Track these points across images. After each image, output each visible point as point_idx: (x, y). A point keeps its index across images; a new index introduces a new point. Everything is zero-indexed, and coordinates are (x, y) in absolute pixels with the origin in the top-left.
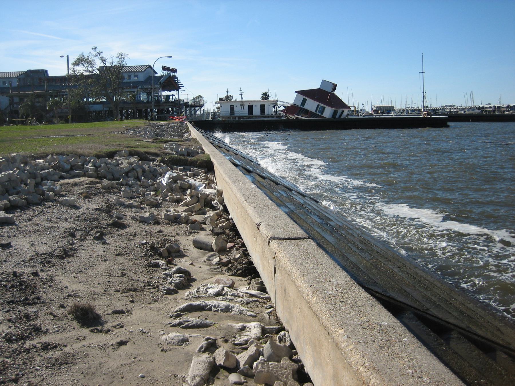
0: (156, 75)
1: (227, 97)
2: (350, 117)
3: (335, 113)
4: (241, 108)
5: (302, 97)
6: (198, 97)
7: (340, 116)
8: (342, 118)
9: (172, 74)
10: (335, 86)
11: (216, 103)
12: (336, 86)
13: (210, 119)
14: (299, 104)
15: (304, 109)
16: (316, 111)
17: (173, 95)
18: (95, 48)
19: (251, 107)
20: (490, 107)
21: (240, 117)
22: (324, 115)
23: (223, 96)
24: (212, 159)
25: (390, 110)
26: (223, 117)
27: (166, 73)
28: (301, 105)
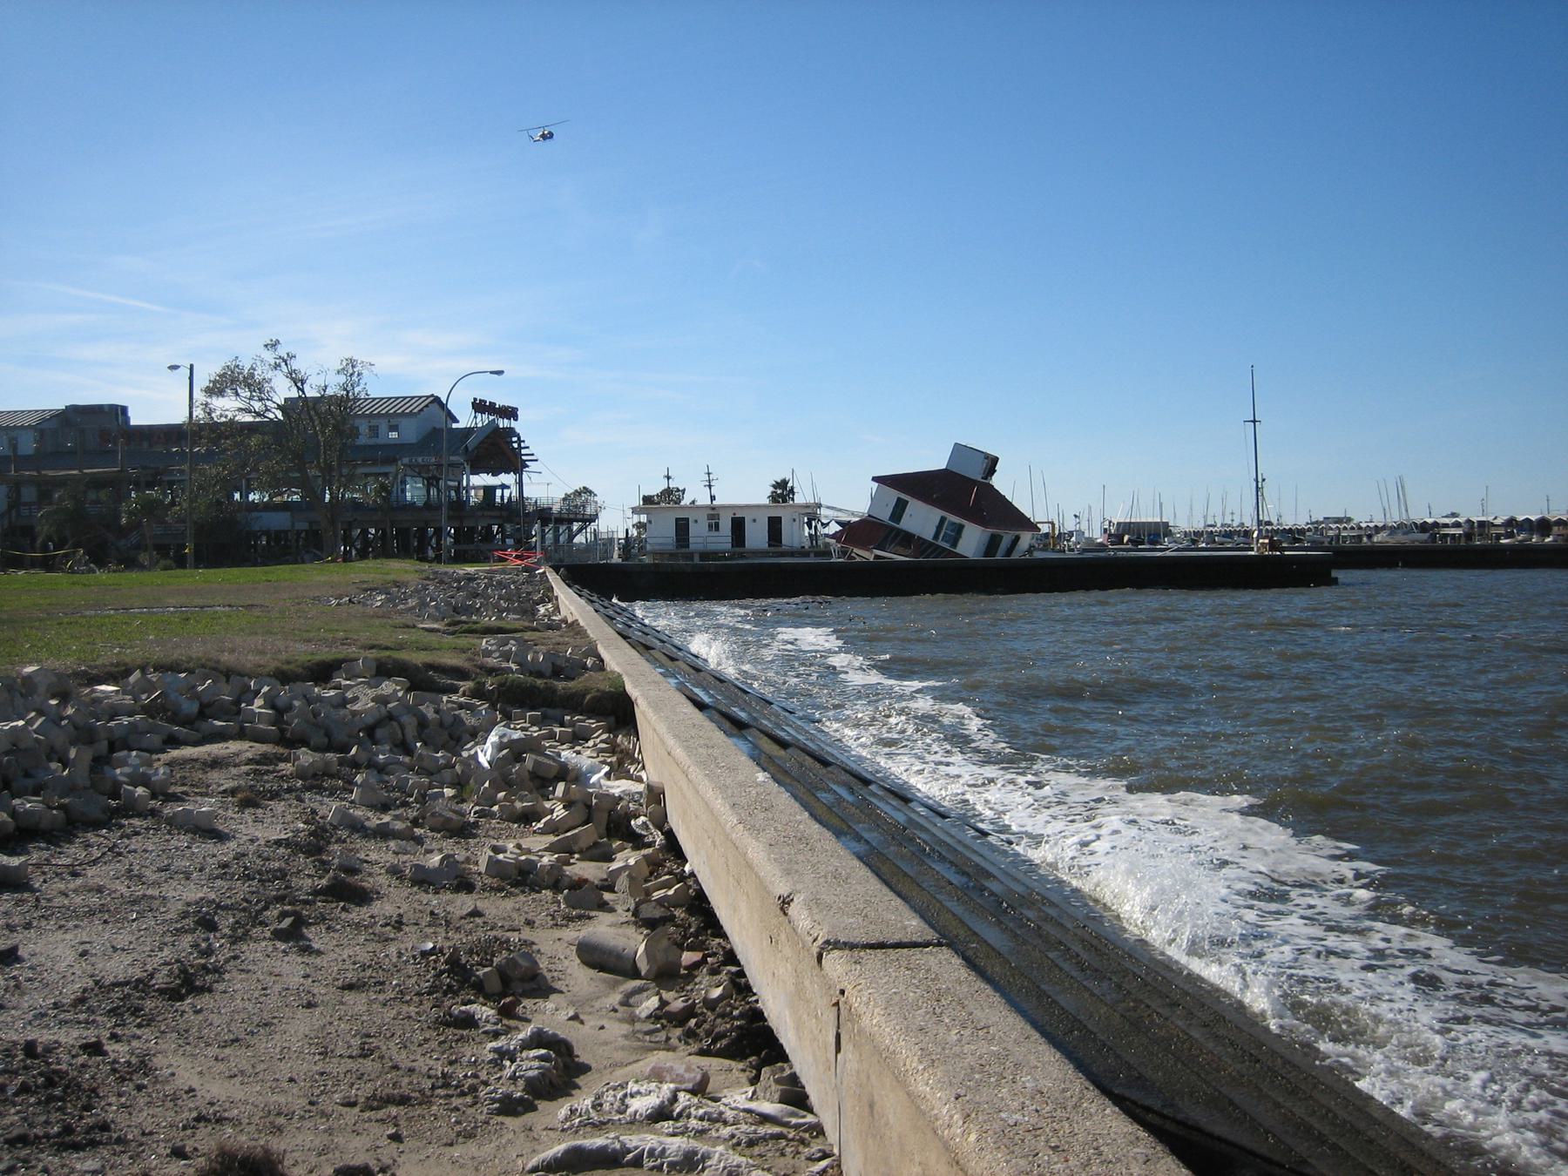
0: (455, 426)
1: (668, 492)
2: (1038, 555)
3: (993, 543)
4: (710, 526)
5: (893, 495)
6: (578, 493)
7: (1009, 552)
8: (1015, 556)
9: (503, 423)
10: (992, 463)
11: (635, 511)
12: (995, 460)
13: (616, 558)
14: (885, 515)
15: (900, 531)
16: (936, 536)
17: (504, 487)
18: (274, 345)
19: (738, 525)
20: (1457, 525)
21: (705, 555)
22: (959, 550)
23: (655, 489)
24: (629, 688)
25: (1158, 531)
26: (654, 553)
27: (483, 420)
28: (892, 518)
